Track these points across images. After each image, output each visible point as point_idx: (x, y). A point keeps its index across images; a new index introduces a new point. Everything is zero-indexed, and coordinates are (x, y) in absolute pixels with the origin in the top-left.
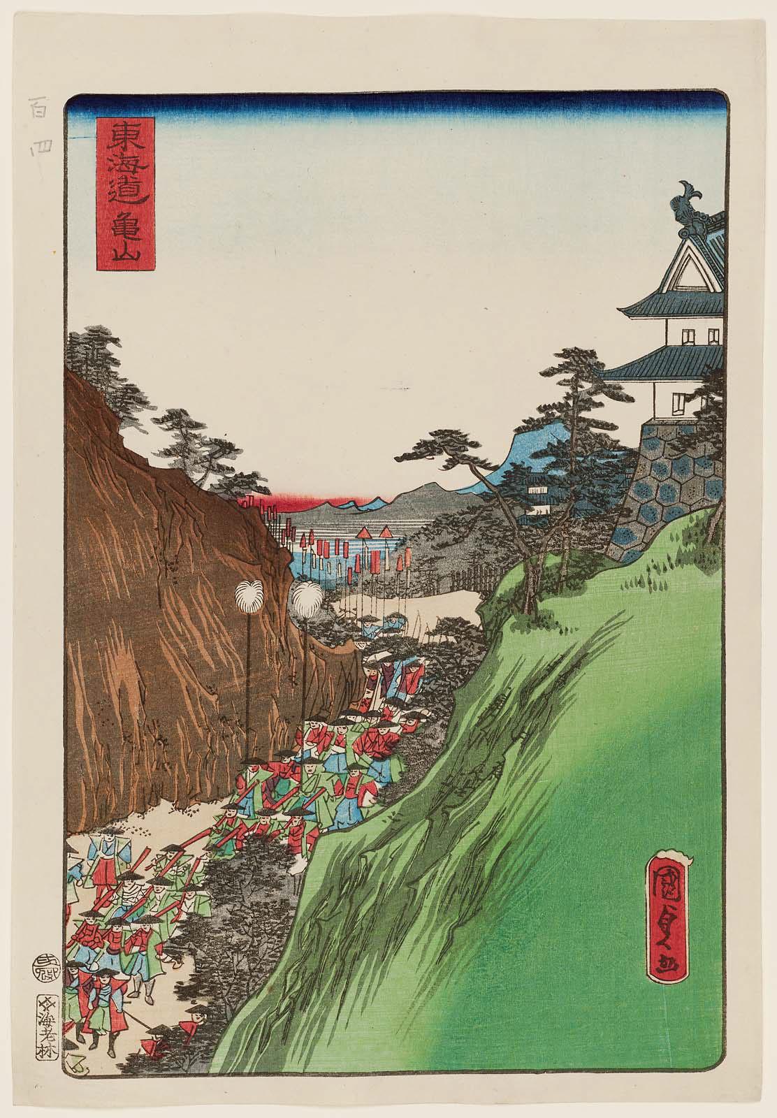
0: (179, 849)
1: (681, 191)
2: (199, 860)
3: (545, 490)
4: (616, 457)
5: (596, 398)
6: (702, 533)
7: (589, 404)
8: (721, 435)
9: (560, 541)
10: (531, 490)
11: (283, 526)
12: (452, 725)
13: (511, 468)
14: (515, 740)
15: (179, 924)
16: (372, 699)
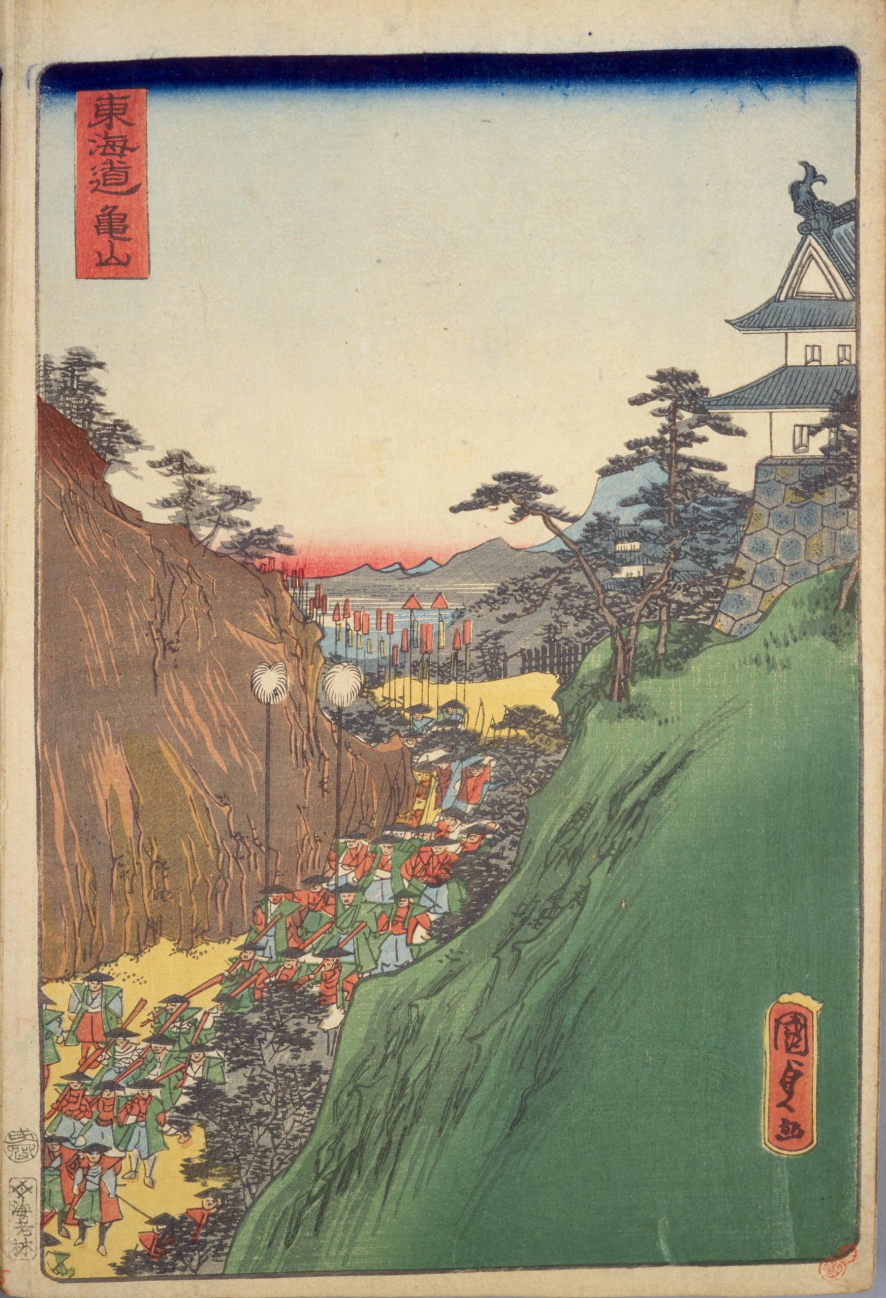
0: (184, 999)
1: (800, 174)
2: (207, 1013)
3: (637, 545)
4: (723, 504)
5: (700, 431)
6: (833, 599)
7: (690, 439)
8: (855, 476)
9: (656, 610)
10: (619, 547)
11: (311, 593)
12: (524, 842)
13: (594, 520)
14: (602, 858)
15: (184, 1091)
16: (423, 810)
